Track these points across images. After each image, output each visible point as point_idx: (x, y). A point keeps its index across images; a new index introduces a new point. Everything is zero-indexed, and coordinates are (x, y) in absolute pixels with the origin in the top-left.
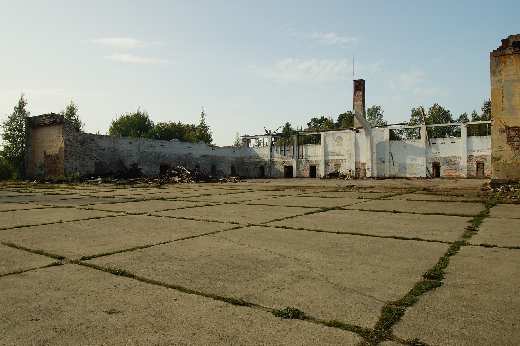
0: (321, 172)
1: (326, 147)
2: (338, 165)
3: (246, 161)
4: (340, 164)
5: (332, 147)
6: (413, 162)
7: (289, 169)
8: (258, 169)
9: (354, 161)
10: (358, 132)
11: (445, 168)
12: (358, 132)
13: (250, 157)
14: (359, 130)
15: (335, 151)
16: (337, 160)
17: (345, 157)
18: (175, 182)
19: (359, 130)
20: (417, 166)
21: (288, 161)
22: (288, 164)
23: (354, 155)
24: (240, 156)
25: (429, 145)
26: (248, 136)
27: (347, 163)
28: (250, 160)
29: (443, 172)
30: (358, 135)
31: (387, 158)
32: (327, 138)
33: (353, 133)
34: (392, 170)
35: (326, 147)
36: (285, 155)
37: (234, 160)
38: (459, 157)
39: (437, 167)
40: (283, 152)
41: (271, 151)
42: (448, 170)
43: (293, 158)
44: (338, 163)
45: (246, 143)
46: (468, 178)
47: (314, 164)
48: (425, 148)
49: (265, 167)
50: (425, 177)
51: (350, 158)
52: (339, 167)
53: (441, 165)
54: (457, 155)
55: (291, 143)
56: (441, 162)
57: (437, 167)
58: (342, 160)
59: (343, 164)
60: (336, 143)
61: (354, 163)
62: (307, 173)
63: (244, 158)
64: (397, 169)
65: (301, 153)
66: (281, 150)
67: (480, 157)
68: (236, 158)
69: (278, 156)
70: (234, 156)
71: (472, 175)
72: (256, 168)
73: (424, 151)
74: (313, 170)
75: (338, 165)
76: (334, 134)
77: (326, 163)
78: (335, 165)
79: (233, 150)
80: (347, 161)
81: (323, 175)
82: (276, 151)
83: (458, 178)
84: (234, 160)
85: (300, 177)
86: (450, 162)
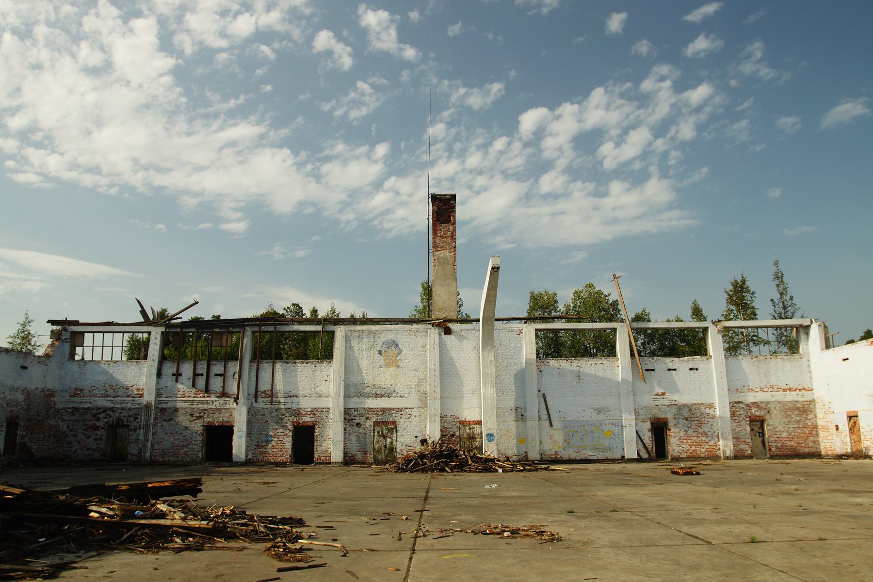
0: (332, 442)
1: (350, 368)
2: (385, 423)
3: (60, 406)
4: (394, 423)
5: (373, 371)
6: (601, 417)
7: (218, 437)
8: (102, 433)
9: (438, 413)
10: (448, 331)
11: (682, 434)
12: (448, 331)
13: (78, 392)
14: (450, 325)
15: (377, 383)
16: (384, 411)
17: (409, 401)
18: (391, 443)
19: (450, 325)
20: (613, 428)
21: (219, 410)
22: (218, 419)
23: (438, 396)
24: (41, 386)
25: (642, 373)
26: (76, 323)
27: (415, 420)
28: (77, 402)
29: (676, 444)
30: (448, 339)
31: (534, 407)
32: (354, 343)
33: (434, 333)
34: (546, 439)
35: (350, 368)
36: (207, 390)
37: (20, 397)
38: (479, 423)
39: (659, 429)
40: (201, 382)
41: (159, 375)
42: (689, 437)
43: (236, 400)
44: (386, 417)
45: (67, 346)
46: (736, 457)
47: (307, 419)
48: (630, 379)
49: (133, 424)
50: (636, 457)
51: (424, 404)
52: (391, 431)
53: (671, 424)
54: (707, 401)
55: (232, 355)
56: (670, 416)
57: (659, 429)
58: (399, 410)
59: (401, 422)
60: (381, 360)
61: (438, 419)
62: (283, 444)
63: (51, 393)
64: (559, 437)
65: (265, 386)
66: (195, 375)
67: (756, 405)
68: (27, 392)
69: (184, 393)
70: (21, 383)
71: (742, 450)
72: (95, 428)
73: (630, 388)
74: (305, 439)
75: (387, 425)
76: (375, 333)
77: (350, 417)
78: (376, 424)
79: (21, 362)
80: (415, 412)
81: (337, 456)
82: (177, 375)
83: (622, 460)
84: (20, 397)
85: (256, 462)
86: (694, 416)
